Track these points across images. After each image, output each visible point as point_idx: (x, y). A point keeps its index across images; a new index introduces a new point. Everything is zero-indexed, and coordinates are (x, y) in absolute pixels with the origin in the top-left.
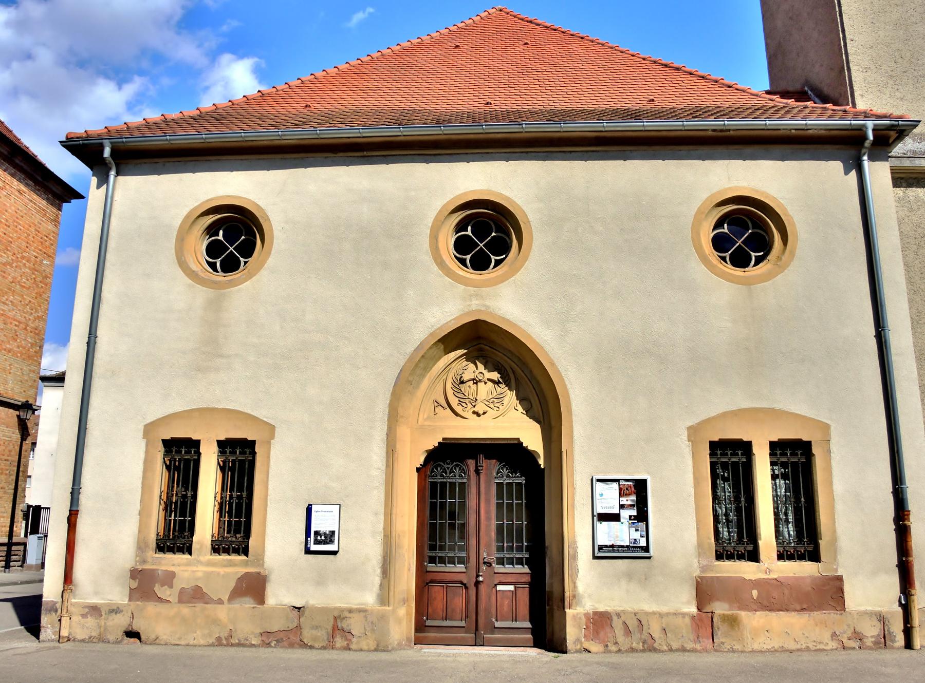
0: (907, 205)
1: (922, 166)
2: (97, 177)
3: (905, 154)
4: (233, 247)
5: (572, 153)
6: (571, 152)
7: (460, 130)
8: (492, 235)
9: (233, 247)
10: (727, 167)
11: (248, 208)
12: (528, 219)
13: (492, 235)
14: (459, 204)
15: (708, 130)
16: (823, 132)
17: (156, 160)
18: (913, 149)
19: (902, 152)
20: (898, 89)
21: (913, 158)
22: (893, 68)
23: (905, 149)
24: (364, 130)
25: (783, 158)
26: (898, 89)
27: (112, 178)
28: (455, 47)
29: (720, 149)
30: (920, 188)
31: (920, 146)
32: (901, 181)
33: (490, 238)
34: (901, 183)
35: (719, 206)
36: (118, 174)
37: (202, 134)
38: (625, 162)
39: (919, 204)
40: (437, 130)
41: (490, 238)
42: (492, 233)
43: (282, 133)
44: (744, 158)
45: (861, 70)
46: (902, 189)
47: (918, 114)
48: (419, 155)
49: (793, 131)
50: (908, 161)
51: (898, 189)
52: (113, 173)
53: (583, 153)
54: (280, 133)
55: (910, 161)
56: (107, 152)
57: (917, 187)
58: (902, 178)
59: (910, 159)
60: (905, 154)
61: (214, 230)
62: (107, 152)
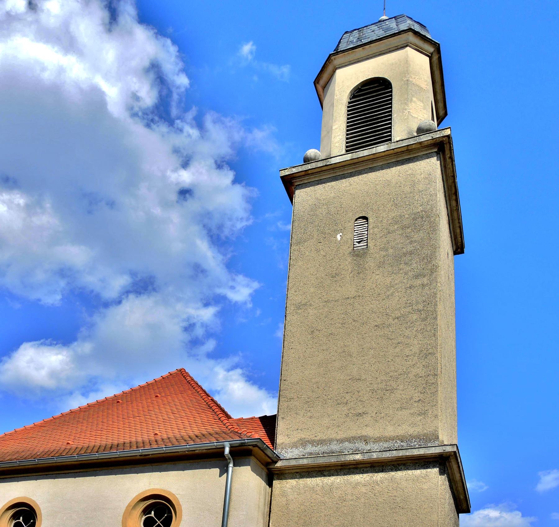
0: (297, 490)
1: (304, 463)
2: (219, 469)
3: (304, 456)
4: (158, 523)
5: (69, 474)
6: (68, 473)
7: (86, 458)
8: (31, 521)
9: (158, 523)
10: (150, 477)
11: (31, 505)
12: (41, 512)
13: (31, 521)
14: (10, 505)
15: (137, 456)
16: (204, 451)
17: (95, 469)
18: (310, 451)
19: (302, 454)
20: (309, 411)
21: (298, 459)
22: (310, 396)
23: (304, 452)
24: (57, 459)
25: (183, 470)
26: (309, 411)
27: (230, 469)
28: (156, 397)
29: (148, 466)
30: (309, 478)
31: (317, 449)
32: (297, 474)
33: (164, 517)
34: (296, 475)
35: (143, 501)
36: (234, 465)
37: (140, 450)
38: (138, 475)
39: (306, 489)
40: (53, 461)
41: (164, 517)
42: (31, 521)
43: (78, 457)
44: (160, 471)
45: (287, 400)
46: (296, 480)
47: (320, 426)
48: (63, 473)
49: (187, 452)
50: (294, 461)
51: (293, 480)
52: (231, 465)
53: (75, 473)
54: (140, 451)
55: (296, 461)
56: (227, 451)
57: (307, 477)
58: (297, 473)
59: (296, 459)
60: (304, 456)
61: (148, 511)
62: (227, 451)
